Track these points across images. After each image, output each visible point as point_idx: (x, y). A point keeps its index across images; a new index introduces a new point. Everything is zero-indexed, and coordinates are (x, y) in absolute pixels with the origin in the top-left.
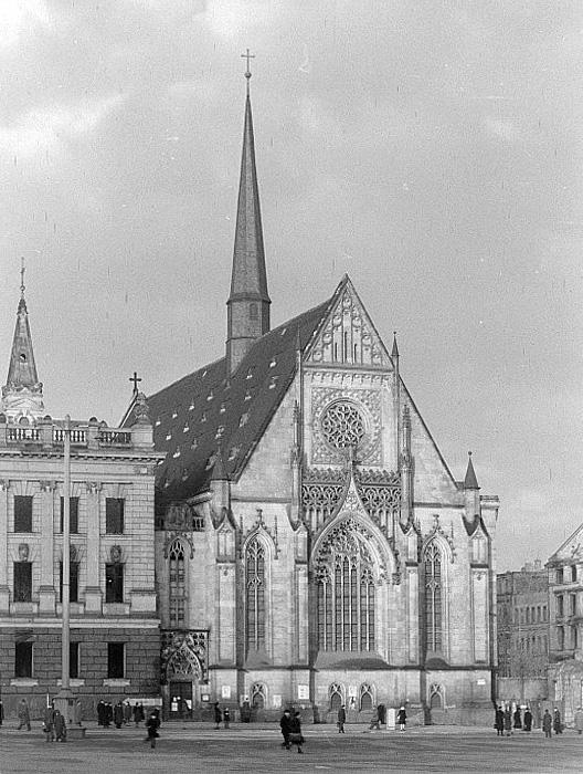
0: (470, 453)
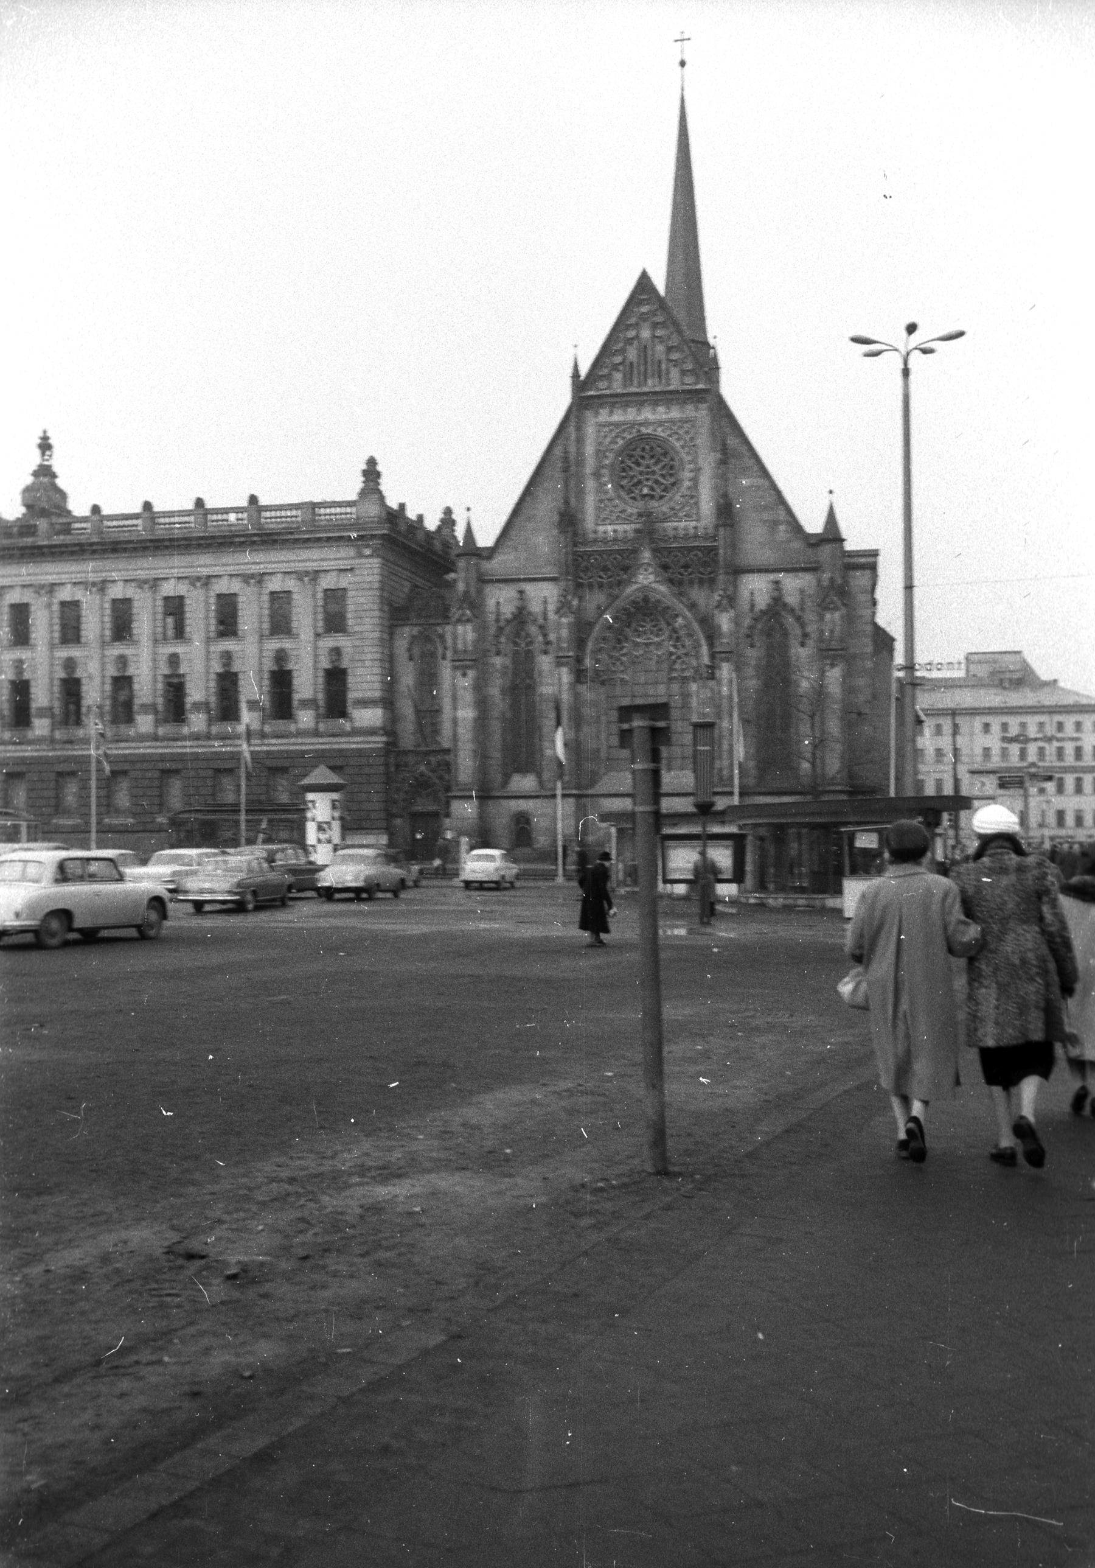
0: (468, 509)
